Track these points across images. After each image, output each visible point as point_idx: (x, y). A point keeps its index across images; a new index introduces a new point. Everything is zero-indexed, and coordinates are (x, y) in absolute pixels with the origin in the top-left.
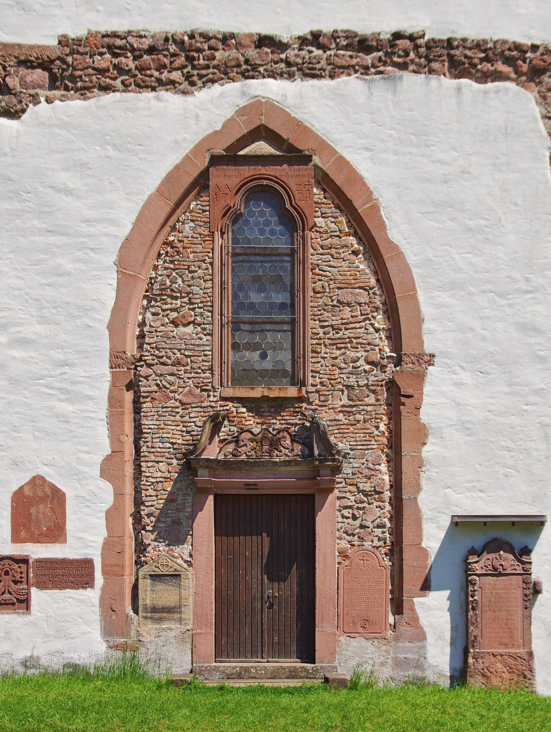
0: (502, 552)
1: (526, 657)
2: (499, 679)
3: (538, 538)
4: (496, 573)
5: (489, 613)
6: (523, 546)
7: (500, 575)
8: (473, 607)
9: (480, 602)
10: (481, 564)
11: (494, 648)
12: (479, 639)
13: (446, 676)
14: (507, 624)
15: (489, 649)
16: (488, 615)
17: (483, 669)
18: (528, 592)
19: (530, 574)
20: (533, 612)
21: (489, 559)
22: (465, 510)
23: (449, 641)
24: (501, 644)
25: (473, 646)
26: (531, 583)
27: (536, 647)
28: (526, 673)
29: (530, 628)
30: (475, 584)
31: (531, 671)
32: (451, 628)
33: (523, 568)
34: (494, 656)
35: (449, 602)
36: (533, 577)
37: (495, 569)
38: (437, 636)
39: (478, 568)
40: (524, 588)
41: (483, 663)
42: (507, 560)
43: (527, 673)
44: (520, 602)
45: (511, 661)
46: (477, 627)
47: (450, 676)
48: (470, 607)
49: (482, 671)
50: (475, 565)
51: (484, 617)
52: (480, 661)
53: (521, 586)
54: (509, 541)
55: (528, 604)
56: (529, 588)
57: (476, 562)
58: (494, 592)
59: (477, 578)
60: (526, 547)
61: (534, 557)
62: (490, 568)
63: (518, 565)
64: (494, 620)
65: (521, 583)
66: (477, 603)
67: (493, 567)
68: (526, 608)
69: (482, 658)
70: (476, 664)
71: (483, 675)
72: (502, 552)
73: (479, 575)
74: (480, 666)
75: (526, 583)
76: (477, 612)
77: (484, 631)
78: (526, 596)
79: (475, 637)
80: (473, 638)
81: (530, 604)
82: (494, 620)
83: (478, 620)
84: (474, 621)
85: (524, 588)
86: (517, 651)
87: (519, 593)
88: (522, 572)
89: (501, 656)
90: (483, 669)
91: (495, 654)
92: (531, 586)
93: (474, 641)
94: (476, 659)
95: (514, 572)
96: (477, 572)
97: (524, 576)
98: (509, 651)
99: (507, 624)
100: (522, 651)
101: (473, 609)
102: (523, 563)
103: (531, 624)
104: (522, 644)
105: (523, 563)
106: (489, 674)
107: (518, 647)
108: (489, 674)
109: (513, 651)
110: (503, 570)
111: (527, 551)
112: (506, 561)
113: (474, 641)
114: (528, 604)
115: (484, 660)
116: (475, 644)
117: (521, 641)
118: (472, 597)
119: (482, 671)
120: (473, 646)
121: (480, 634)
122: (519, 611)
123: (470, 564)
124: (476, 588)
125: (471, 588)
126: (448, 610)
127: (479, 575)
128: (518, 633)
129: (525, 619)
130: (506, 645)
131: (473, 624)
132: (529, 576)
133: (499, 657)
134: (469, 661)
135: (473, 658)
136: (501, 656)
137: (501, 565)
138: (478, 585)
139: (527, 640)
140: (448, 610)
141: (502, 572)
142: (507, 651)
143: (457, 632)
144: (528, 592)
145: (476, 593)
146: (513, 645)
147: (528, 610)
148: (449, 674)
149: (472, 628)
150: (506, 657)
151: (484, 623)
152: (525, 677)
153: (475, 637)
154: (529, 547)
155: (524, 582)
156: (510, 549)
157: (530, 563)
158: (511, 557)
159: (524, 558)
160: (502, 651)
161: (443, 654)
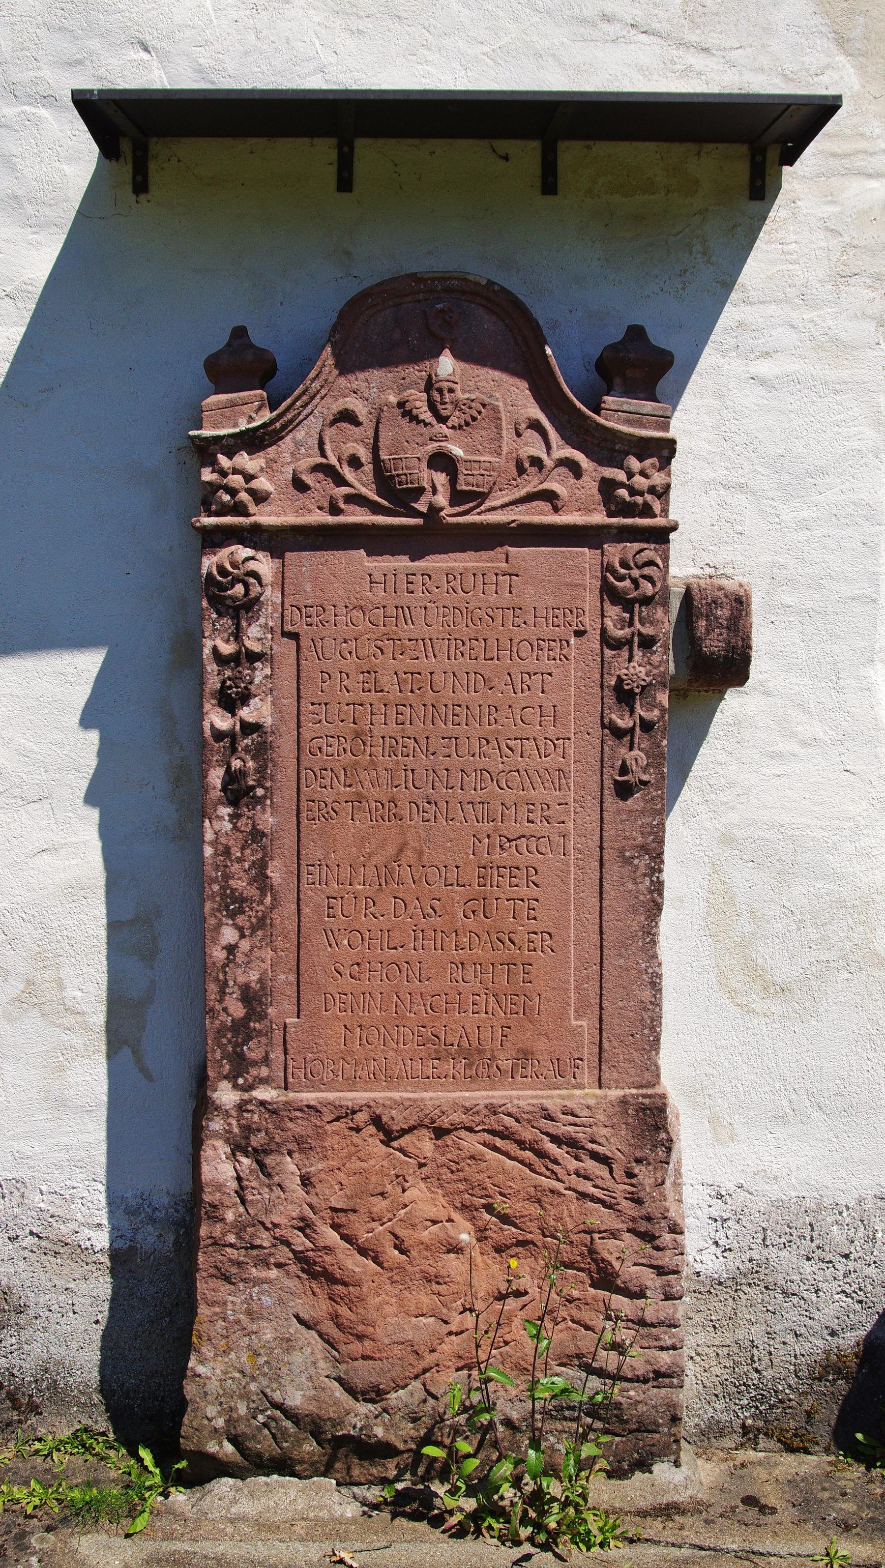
0: (446, 365)
1: (613, 1144)
2: (424, 1298)
3: (726, 284)
4: (409, 523)
5: (351, 827)
6: (616, 334)
7: (433, 537)
8: (232, 777)
9: (285, 748)
10: (295, 452)
11: (391, 1080)
12: (280, 1010)
13: (82, 1252)
14: (479, 905)
15: (352, 1084)
16: (348, 836)
17: (305, 1226)
18: (636, 669)
19: (661, 536)
20: (674, 824)
21: (347, 417)
22: (200, 70)
23: (99, 1018)
24: (438, 1049)
25: (239, 1066)
26: (663, 598)
27: (678, 1068)
28: (608, 1249)
29: (650, 935)
30: (249, 606)
31: (648, 1237)
32: (113, 926)
33: (607, 487)
34: (389, 1136)
35: (94, 736)
36: (684, 564)
37: (396, 492)
38: (16, 986)
39: (273, 486)
40: (606, 640)
41: (306, 1181)
42: (490, 420)
43: (623, 1253)
44: (580, 751)
45: (505, 1168)
46: (261, 923)
47: (115, 1255)
48: (216, 777)
49: (300, 1241)
50: (243, 460)
51: (313, 851)
52: (289, 1167)
53: (590, 622)
54: (513, 284)
55: (636, 757)
56: (647, 643)
57: (255, 441)
58: (388, 666)
59: (265, 565)
60: (636, 333)
61: (693, 419)
62: (361, 482)
63: (576, 470)
64: (387, 876)
65: (590, 600)
66: (261, 751)
67: (383, 479)
68: (624, 791)
69: (302, 1145)
70: (259, 1194)
71: (314, 1269)
72: (446, 365)
73: (277, 541)
74: (288, 1205)
75: (628, 605)
76: (267, 820)
77: (320, 954)
78: (625, 696)
79: (248, 996)
80: (238, 1010)
81: (656, 758)
82: (387, 876)
83: (275, 873)
84: (239, 884)
85: (606, 640)
86: (553, 1099)
87: (573, 681)
88: (599, 518)
89: (440, 1133)
90: (305, 1226)
91: (398, 1119)
92: (665, 622)
93: (242, 1030)
94: (258, 1155)
95: (540, 515)
96: (264, 517)
97: (614, 552)
98: (497, 1095)
99: (479, 905)
100: (588, 1098)
101: (237, 792)
102: (608, 448)
103: (655, 909)
104: (588, 1051)
105: (608, 448)
106: (355, 1264)
107: (564, 1070)
108: (355, 1264)
109: (521, 1096)
110: (457, 497)
111: (647, 366)
112: (481, 433)
113: (242, 1030)
114: (636, 757)
115: (316, 1167)
116: (253, 1051)
117: (585, 1024)
118: (230, 702)
119: (300, 1241)
120: (239, 1066)
121: (286, 978)
122: (577, 812)
123: (206, 451)
124: (254, 636)
125: (217, 641)
126: (91, 798)
127: (277, 541)
128: (563, 972)
129: (614, 869)
130: (475, 1061)
131: (233, 905)
132: (650, 553)
133: (424, 1144)
134: (207, 1172)
135: (238, 1148)
136: (440, 1133)
137: (442, 461)
138: (268, 616)
139: (629, 1022)
140: (91, 798)
141: (449, 515)
142: (480, 1096)
143: (149, 956)
144: (636, 669)
145: (261, 672)
146: (526, 1055)
147: (635, 801)
148: (102, 1240)
149: (229, 935)
150: (471, 1143)
151: (314, 896)
152: (605, 1278)
153: (248, 996)
154: (658, 338)
155: (609, 593)
156: (516, 343)
157: (664, 451)
158: (515, 398)
159: (619, 414)
160: (449, 1096)
161: (59, 1104)
